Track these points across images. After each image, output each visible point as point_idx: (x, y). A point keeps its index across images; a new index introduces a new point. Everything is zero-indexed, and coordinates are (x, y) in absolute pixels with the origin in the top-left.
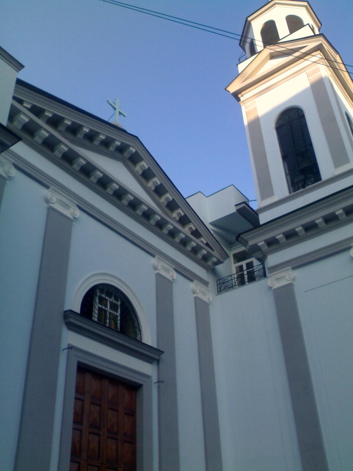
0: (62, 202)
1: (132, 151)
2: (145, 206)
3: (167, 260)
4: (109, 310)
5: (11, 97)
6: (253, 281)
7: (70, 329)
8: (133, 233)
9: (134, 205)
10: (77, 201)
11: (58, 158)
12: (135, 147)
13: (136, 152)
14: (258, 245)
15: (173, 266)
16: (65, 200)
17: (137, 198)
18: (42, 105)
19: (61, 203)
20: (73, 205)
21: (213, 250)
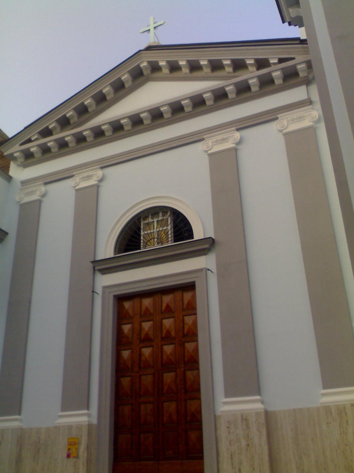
0: (83, 178)
1: (144, 66)
2: (163, 108)
3: (95, 166)
4: (155, 231)
5: (308, 41)
6: (134, 115)
7: (103, 274)
8: (165, 140)
9: (199, 103)
10: (97, 165)
11: (74, 147)
12: (143, 60)
13: (149, 62)
14: (159, 63)
15: (232, 129)
16: (219, 137)
17: (192, 97)
18: (54, 118)
19: (217, 143)
20: (232, 133)
21: (294, 59)
